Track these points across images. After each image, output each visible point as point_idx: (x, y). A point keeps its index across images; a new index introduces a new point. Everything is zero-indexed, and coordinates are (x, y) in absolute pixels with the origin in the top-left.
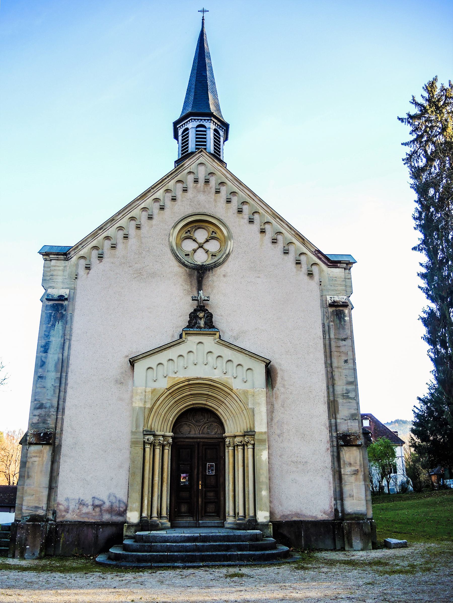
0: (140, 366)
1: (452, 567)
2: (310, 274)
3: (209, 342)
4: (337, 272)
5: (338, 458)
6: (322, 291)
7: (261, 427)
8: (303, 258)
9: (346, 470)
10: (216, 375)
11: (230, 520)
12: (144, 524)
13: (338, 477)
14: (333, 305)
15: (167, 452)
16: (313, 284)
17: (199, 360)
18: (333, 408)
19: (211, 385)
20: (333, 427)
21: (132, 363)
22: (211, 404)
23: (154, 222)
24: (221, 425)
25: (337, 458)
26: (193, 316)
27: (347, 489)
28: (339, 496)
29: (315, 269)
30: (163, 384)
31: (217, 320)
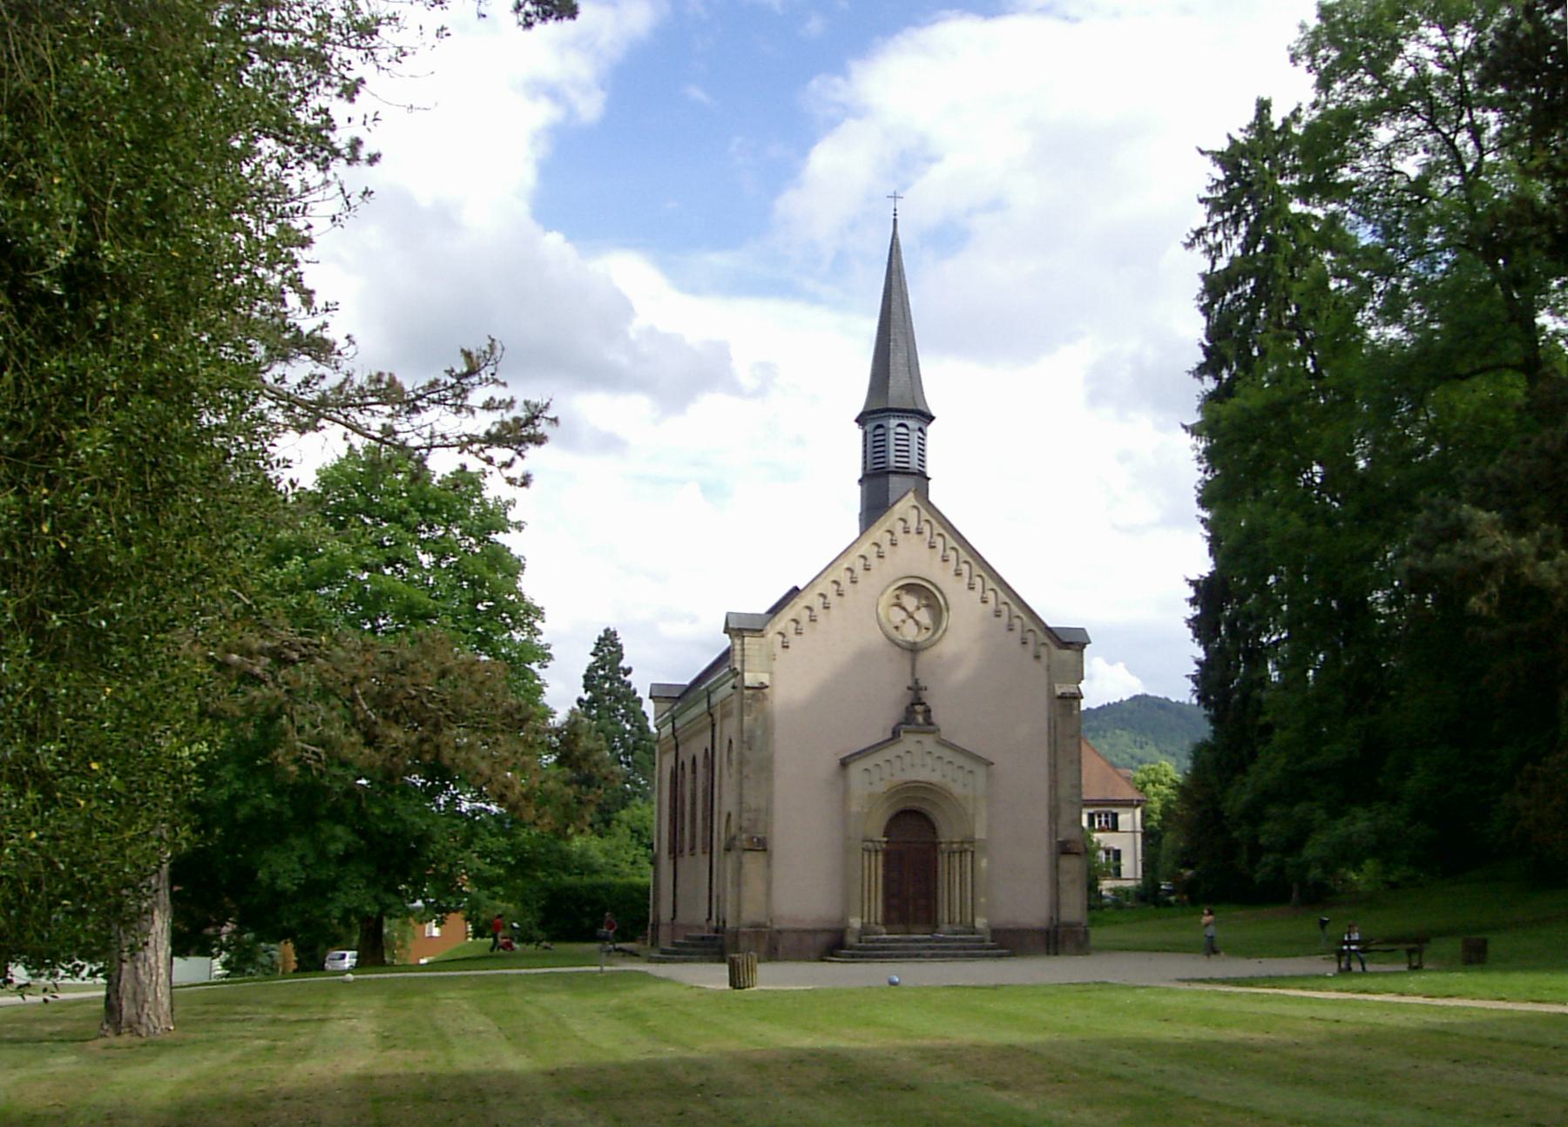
0: (855, 770)
1: (348, 3)
2: (1037, 657)
3: (928, 740)
4: (1067, 654)
5: (1057, 867)
6: (1049, 677)
7: (980, 834)
8: (1030, 636)
9: (1064, 879)
10: (935, 778)
11: (946, 927)
12: (865, 930)
13: (1056, 884)
14: (1062, 697)
15: (880, 857)
16: (1040, 668)
17: (918, 763)
18: (1054, 814)
19: (927, 788)
20: (1053, 831)
21: (844, 764)
22: (925, 807)
23: (858, 586)
24: (932, 828)
25: (1056, 867)
26: (910, 712)
27: (1063, 899)
28: (1056, 905)
29: (1043, 651)
30: (881, 788)
31: (936, 717)
